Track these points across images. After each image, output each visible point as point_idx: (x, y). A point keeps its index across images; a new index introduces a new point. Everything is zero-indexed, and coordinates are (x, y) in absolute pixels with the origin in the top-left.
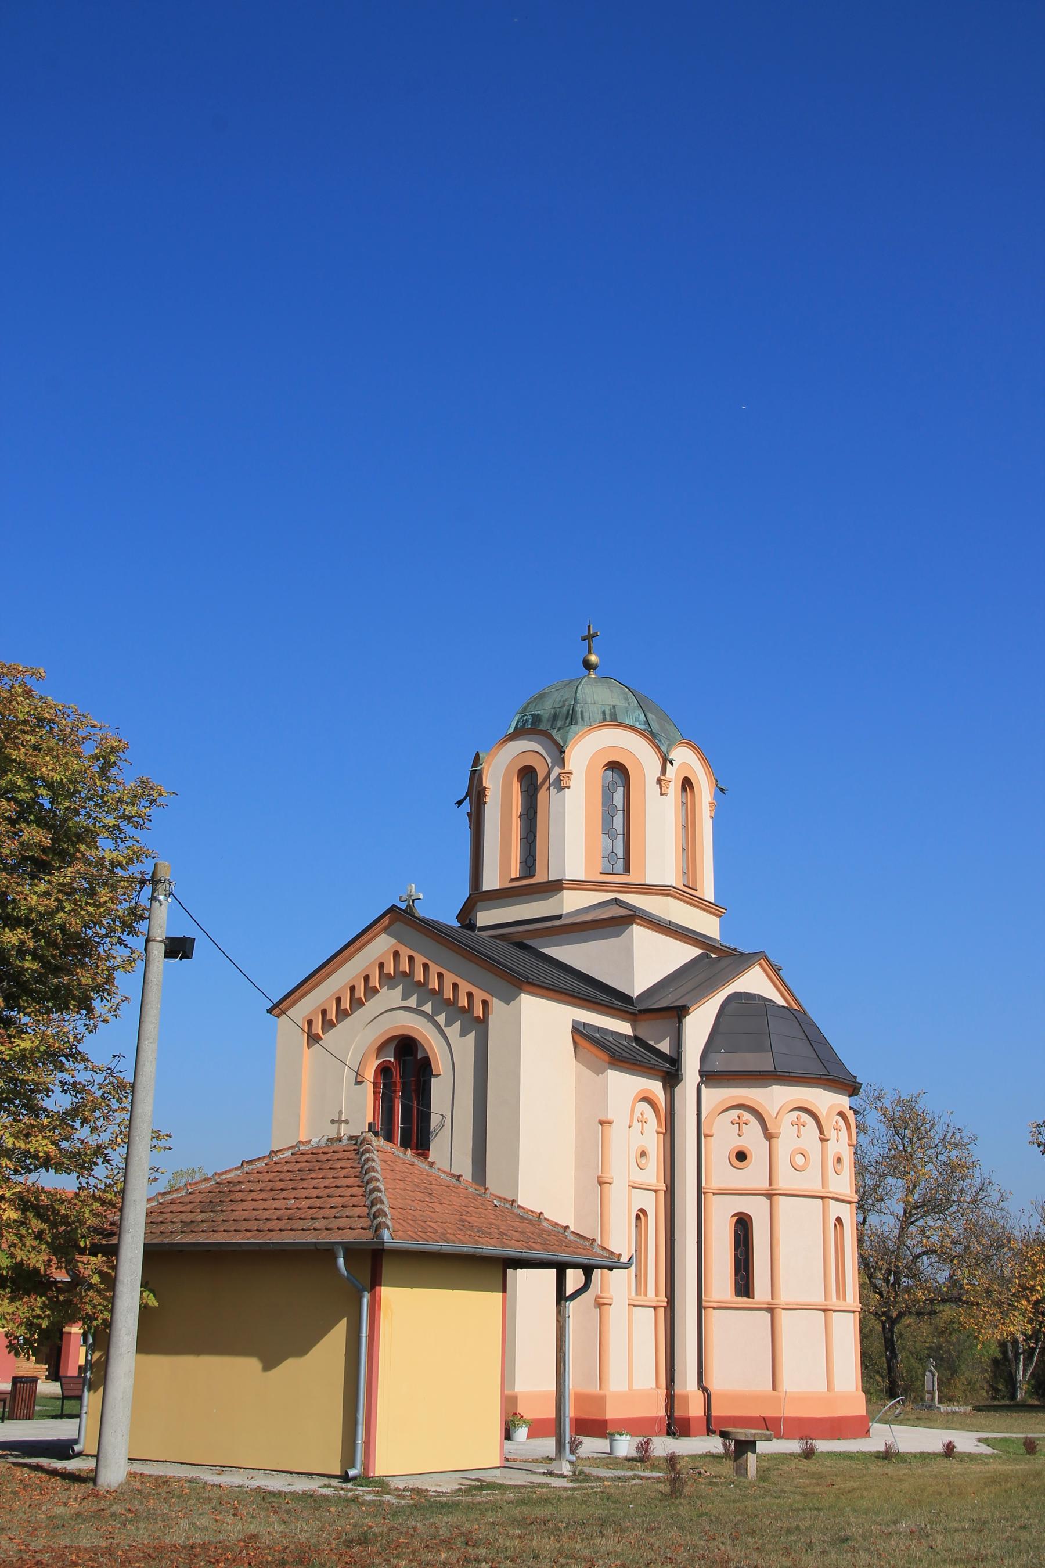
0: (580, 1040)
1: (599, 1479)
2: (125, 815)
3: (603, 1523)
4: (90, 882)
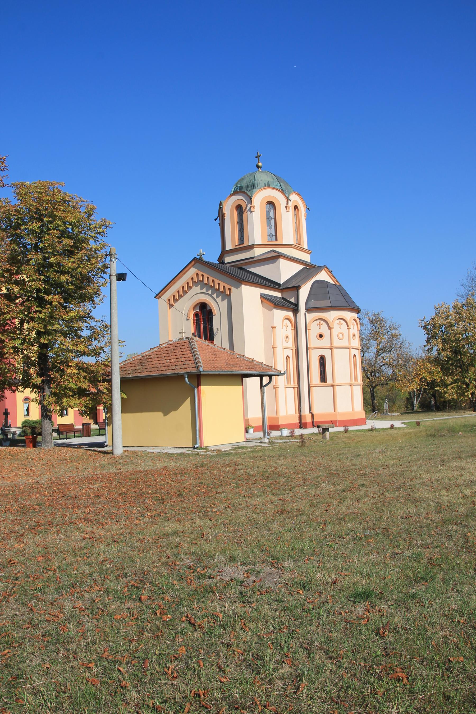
0: (263, 300)
1: (278, 443)
2: (98, 232)
3: (280, 456)
4: (88, 257)
